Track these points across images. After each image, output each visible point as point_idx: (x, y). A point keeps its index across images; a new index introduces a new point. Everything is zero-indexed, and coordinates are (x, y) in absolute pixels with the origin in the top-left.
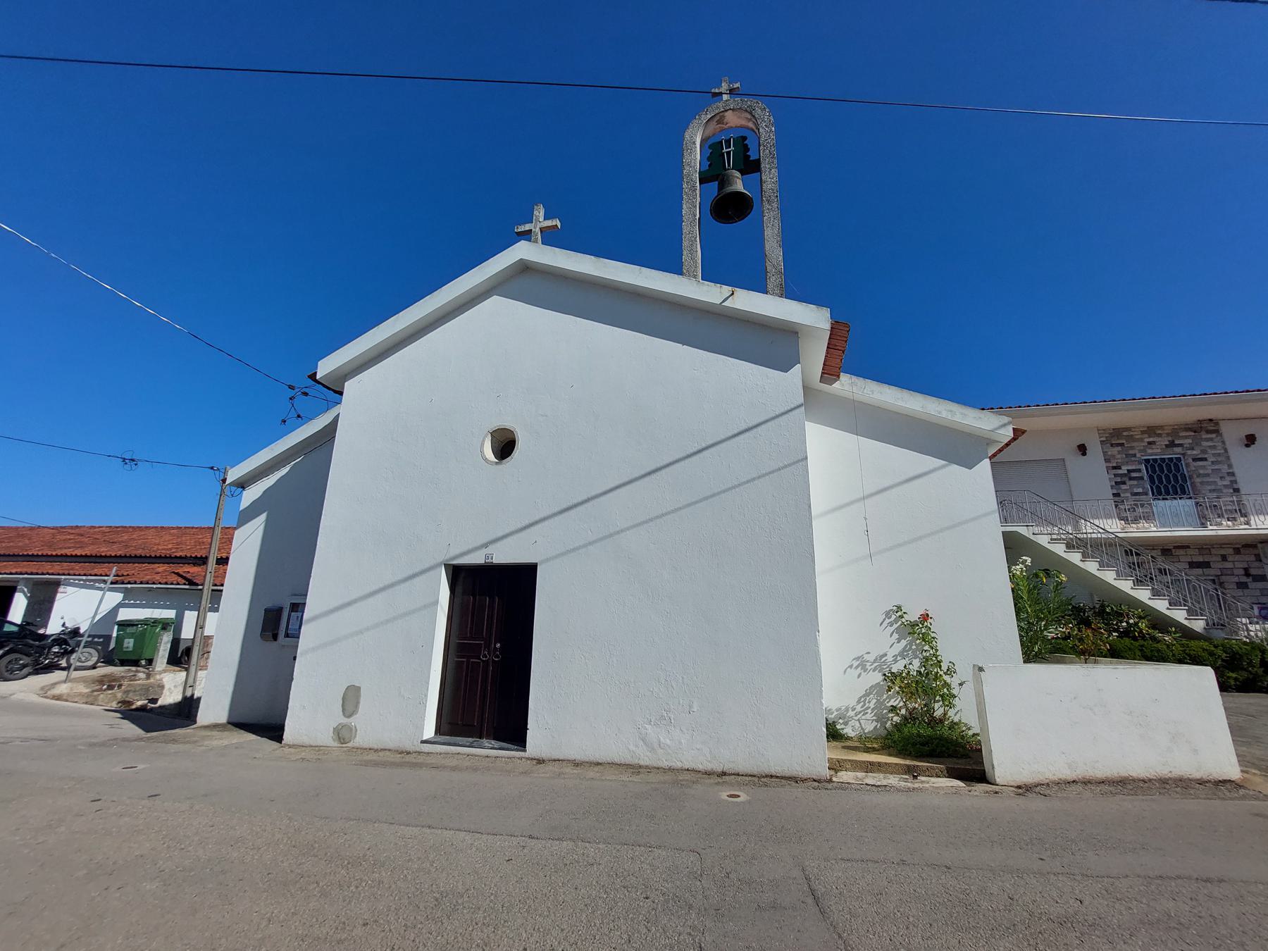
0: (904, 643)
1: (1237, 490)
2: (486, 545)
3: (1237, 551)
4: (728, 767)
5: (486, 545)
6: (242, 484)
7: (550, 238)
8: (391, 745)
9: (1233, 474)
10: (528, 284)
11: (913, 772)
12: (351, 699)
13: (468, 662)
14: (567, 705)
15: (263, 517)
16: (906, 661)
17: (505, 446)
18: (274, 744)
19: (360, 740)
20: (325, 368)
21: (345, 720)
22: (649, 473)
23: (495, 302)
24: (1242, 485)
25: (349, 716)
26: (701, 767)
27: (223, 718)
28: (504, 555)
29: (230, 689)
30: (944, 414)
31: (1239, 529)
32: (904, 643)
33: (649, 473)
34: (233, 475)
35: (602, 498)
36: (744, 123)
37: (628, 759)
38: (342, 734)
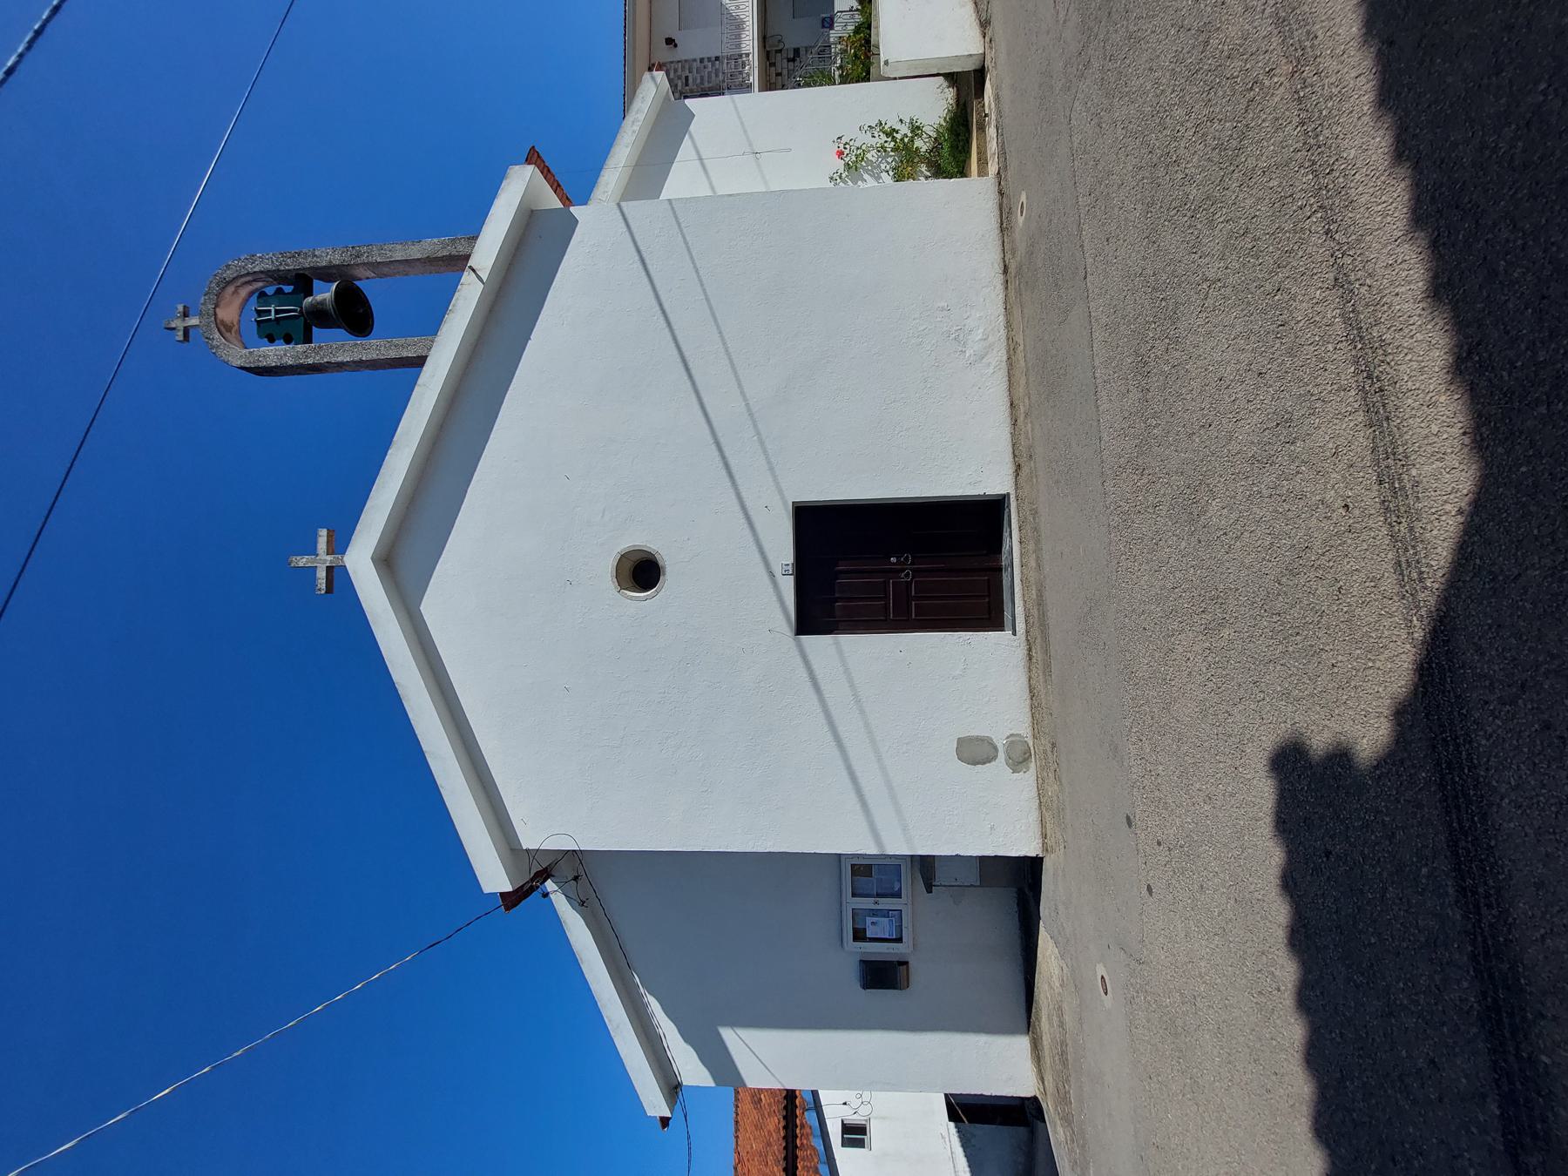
0: (866, 176)
1: (717, 58)
2: (772, 575)
3: (773, 64)
4: (999, 268)
5: (772, 575)
6: (673, 1089)
7: (339, 544)
8: (1024, 680)
9: (702, 60)
10: (405, 564)
11: (982, 128)
12: (975, 751)
13: (917, 598)
14: (958, 457)
15: (727, 1034)
16: (884, 175)
17: (642, 572)
18: (1048, 867)
19: (1023, 728)
20: (495, 878)
21: (1001, 755)
22: (687, 369)
23: (430, 608)
24: (713, 55)
25: (995, 748)
26: (1002, 296)
27: (1022, 1043)
28: (783, 550)
29: (982, 1039)
30: (636, 128)
31: (754, 60)
32: (866, 176)
33: (687, 369)
34: (655, 1104)
35: (715, 424)
36: (238, 302)
37: (1003, 373)
38: (1018, 762)
